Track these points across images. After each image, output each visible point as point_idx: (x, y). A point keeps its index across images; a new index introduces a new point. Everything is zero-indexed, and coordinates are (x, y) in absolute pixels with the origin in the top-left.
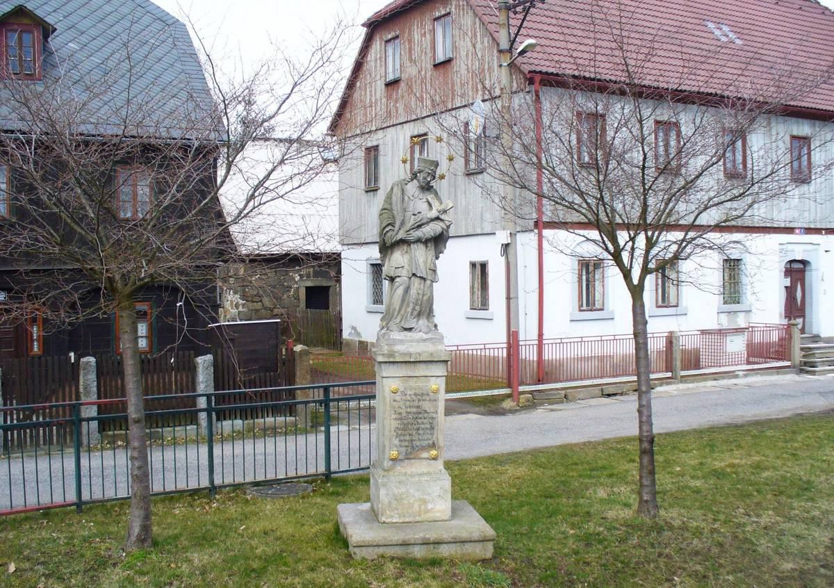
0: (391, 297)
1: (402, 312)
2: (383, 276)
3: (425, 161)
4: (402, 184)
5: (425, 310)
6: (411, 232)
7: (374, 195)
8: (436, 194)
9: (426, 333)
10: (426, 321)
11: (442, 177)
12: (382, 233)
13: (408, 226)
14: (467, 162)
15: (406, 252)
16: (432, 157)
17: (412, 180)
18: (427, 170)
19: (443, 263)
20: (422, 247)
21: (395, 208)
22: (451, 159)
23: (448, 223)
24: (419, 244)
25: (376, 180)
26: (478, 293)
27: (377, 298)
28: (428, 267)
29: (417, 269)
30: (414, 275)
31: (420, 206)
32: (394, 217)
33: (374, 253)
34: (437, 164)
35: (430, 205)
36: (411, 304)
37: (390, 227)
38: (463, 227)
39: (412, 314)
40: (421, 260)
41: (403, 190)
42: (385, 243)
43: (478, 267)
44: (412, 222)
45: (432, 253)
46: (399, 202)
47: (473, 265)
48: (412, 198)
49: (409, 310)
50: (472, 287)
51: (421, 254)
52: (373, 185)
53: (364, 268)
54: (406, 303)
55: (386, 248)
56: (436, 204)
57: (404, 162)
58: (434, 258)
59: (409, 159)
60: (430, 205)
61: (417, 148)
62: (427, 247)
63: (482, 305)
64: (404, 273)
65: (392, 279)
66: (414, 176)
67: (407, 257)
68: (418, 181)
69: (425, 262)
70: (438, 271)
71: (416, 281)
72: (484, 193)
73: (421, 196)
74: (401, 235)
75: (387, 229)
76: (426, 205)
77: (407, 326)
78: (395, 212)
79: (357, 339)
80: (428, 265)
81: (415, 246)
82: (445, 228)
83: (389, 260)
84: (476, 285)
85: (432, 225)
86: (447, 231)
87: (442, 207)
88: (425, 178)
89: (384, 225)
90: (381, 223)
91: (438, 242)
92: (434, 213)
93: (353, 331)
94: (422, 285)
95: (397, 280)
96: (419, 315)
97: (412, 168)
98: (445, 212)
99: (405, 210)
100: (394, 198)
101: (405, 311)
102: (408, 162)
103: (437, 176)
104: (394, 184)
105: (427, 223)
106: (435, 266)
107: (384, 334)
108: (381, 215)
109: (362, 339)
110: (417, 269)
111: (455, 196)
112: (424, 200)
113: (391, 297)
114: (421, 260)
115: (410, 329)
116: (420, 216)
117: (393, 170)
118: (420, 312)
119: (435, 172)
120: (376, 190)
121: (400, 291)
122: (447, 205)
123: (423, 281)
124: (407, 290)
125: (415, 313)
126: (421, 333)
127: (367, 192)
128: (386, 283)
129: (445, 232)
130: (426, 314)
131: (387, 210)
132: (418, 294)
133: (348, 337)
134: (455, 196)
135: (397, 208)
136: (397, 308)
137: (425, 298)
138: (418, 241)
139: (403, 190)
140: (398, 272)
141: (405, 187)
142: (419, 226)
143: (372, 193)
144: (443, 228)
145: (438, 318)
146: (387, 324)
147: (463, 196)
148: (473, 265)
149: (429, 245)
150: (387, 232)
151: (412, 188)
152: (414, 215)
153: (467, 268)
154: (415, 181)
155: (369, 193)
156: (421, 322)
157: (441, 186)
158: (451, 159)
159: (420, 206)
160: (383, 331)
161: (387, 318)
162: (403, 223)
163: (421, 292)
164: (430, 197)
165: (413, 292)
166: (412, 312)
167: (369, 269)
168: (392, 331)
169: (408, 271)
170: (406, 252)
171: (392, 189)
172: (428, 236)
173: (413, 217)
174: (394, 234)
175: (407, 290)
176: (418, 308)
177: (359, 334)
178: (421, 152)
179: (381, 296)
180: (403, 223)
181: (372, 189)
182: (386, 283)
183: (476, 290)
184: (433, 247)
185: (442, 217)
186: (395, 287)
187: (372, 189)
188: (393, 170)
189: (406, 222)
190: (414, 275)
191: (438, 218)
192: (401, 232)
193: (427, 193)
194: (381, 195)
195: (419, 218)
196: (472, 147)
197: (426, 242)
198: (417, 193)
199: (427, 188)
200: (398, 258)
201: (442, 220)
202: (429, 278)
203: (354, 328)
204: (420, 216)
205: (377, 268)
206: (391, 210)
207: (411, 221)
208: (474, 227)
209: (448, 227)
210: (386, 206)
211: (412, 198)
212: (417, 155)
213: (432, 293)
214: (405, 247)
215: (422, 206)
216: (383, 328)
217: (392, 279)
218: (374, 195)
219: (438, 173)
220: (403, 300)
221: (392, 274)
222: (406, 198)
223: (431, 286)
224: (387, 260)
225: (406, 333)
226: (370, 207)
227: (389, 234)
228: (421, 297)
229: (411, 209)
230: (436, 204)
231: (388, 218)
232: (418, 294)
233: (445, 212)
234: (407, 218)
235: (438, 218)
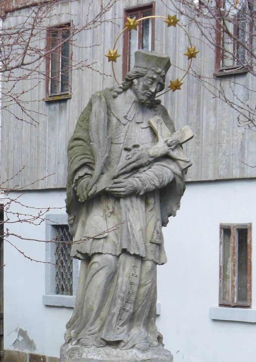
0: (86, 286)
1: (103, 314)
2: (73, 253)
3: (148, 58)
4: (108, 97)
5: (143, 311)
6: (121, 179)
7: (61, 108)
8: (165, 114)
9: (144, 351)
10: (143, 330)
11: (176, 86)
12: (73, 179)
13: (116, 169)
14: (220, 55)
15: (112, 213)
16: (160, 52)
17: (125, 90)
18: (150, 74)
19: (175, 231)
20: (138, 203)
21: (94, 136)
22: (191, 55)
23: (184, 165)
24: (134, 199)
25: (65, 83)
26: (233, 279)
27: (63, 284)
28: (149, 239)
29: (129, 241)
30: (124, 251)
31: (138, 134)
32: (92, 153)
33: (57, 206)
34: (167, 64)
35: (154, 133)
36: (119, 301)
37: (86, 170)
38: (211, 166)
39: (119, 318)
40: (137, 227)
41: (108, 107)
42: (77, 197)
43: (235, 234)
44: (123, 162)
45: (155, 215)
46: (101, 126)
47: (226, 231)
48: (124, 121)
49: (116, 310)
50: (223, 269)
51: (136, 215)
52: (59, 91)
53: (41, 232)
54: (109, 300)
55: (78, 205)
56: (163, 132)
57: (112, 58)
58: (159, 223)
59: (120, 52)
60: (154, 133)
61: (135, 35)
62: (147, 204)
63: (239, 298)
64: (107, 248)
65: (87, 258)
66: (129, 84)
67: (112, 221)
68: (136, 93)
69: (144, 230)
70: (166, 246)
71: (128, 263)
72: (242, 118)
73: (139, 118)
74: (104, 184)
75: (81, 173)
76: (146, 134)
77: (112, 338)
78: (95, 145)
79: (27, 351)
80: (149, 236)
81: (128, 202)
82: (179, 172)
83: (84, 225)
84: (230, 265)
85: (157, 168)
86: (182, 178)
87: (176, 137)
88: (146, 88)
89: (76, 166)
90: (71, 162)
91: (167, 196)
92: (160, 148)
93: (21, 338)
94: (138, 270)
95: (96, 259)
96: (132, 320)
97: (126, 67)
98: (179, 145)
99: (111, 142)
100: (93, 120)
101: (109, 312)
102: (120, 60)
103: (167, 84)
104: (94, 96)
105: (149, 164)
106: (161, 237)
107: (73, 349)
108: (70, 148)
109: (36, 352)
110: (129, 241)
111: (198, 113)
112: (145, 125)
113: (86, 286)
114: (137, 227)
115: (116, 344)
116: (137, 152)
117: (94, 72)
118: (133, 314)
119: (164, 77)
120: (65, 100)
121: (100, 279)
122: (183, 132)
123: (139, 263)
124: (112, 277)
125: (126, 316)
126: (135, 351)
127: (49, 103)
128: (78, 265)
129: (178, 181)
130: (144, 318)
131: (80, 141)
132: (131, 284)
133: (12, 348)
134: (198, 113)
135: (98, 138)
136: (95, 308)
137: (143, 290)
138: (134, 194)
139: (108, 107)
140: (98, 246)
141: (111, 101)
142: (136, 169)
143: (57, 106)
144: (174, 173)
145: (161, 325)
146: (78, 333)
147: (211, 113)
148: (226, 231)
149: (151, 201)
150: (81, 177)
151: (125, 104)
152: (126, 149)
153: (216, 236)
154: (129, 92)
155: (53, 106)
156: (135, 331)
157: (174, 102)
158: (191, 55)
159: (138, 134)
160: (70, 346)
161: (77, 326)
162: (107, 164)
163: (136, 281)
164: (155, 120)
165: (122, 280)
166: (120, 315)
167: (51, 234)
168: (86, 346)
169: (115, 245)
170: (112, 213)
171: (90, 104)
172: (149, 186)
173: (125, 153)
174: (92, 181)
175: (112, 277)
176: (129, 307)
177: (30, 343)
178: (142, 45)
179: (70, 280)
180: (107, 164)
181: (57, 99)
182: (78, 265)
183: (229, 273)
184: (158, 205)
185: (175, 154)
186: (92, 271)
187: (57, 99)
188: (94, 72)
189: (113, 162)
190: (124, 251)
191: (166, 157)
192: (105, 178)
193: (150, 112)
194: (74, 109)
195: (134, 155)
196: (231, 27)
197: (145, 196)
198: (133, 112)
199: (149, 104)
200: (97, 220)
201: (174, 160)
202: (151, 256)
203: (22, 333)
204: (137, 152)
205: (63, 234)
206: (88, 141)
207: (123, 160)
208: (229, 168)
209: (184, 171)
210: (80, 134)
211: (124, 121)
212: (135, 47)
213: (154, 282)
214: (110, 204)
215: (141, 135)
216: (70, 341)
217: (87, 258)
218: (61, 108)
219: (170, 76)
220: (105, 294)
221: (87, 248)
222: (114, 121)
223: (153, 271)
224: (80, 225)
225: (108, 349)
226: (53, 129)
227: (83, 182)
228: (135, 288)
229: (122, 140)
230: (163, 132)
231: (83, 152)
232: (131, 284)
233: (179, 145)
234: (114, 156)
235: (166, 157)
